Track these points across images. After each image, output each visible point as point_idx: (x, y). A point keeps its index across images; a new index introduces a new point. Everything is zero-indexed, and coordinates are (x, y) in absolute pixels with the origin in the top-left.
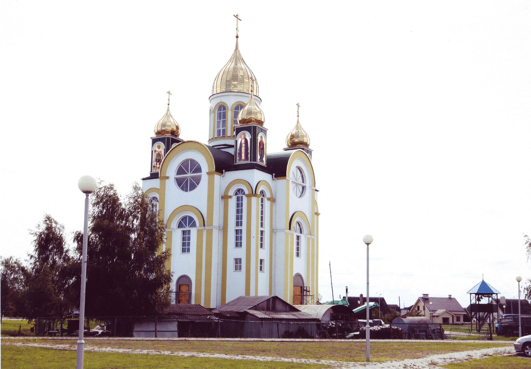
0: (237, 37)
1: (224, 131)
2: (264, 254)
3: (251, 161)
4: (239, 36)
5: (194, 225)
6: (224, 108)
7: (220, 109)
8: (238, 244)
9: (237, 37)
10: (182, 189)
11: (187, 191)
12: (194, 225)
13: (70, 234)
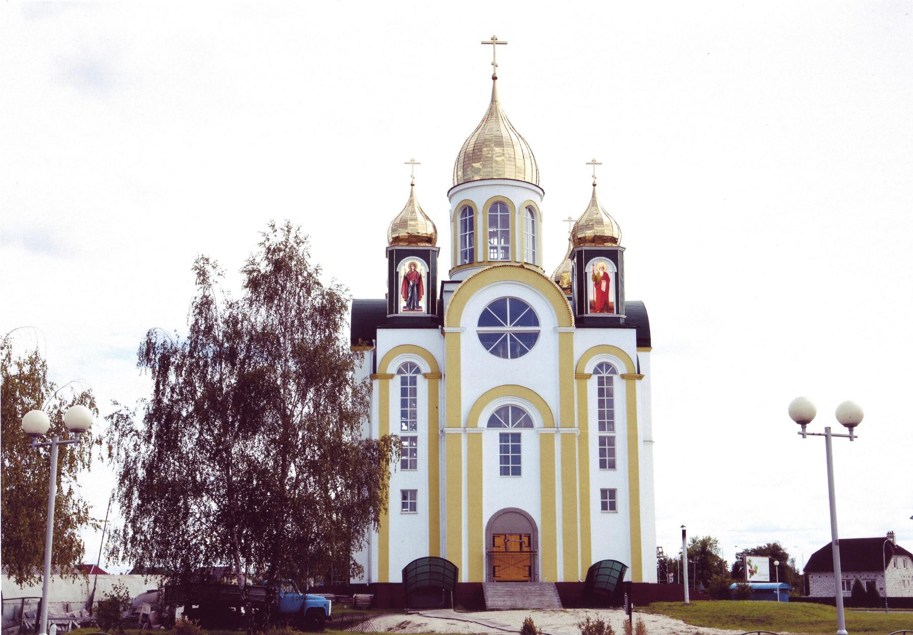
0: (494, 78)
1: (472, 252)
2: (616, 479)
3: (618, 313)
4: (497, 75)
5: (528, 423)
6: (471, 212)
7: (464, 213)
8: (607, 463)
9: (494, 78)
10: (495, 352)
11: (505, 356)
12: (528, 423)
13: (137, 405)
